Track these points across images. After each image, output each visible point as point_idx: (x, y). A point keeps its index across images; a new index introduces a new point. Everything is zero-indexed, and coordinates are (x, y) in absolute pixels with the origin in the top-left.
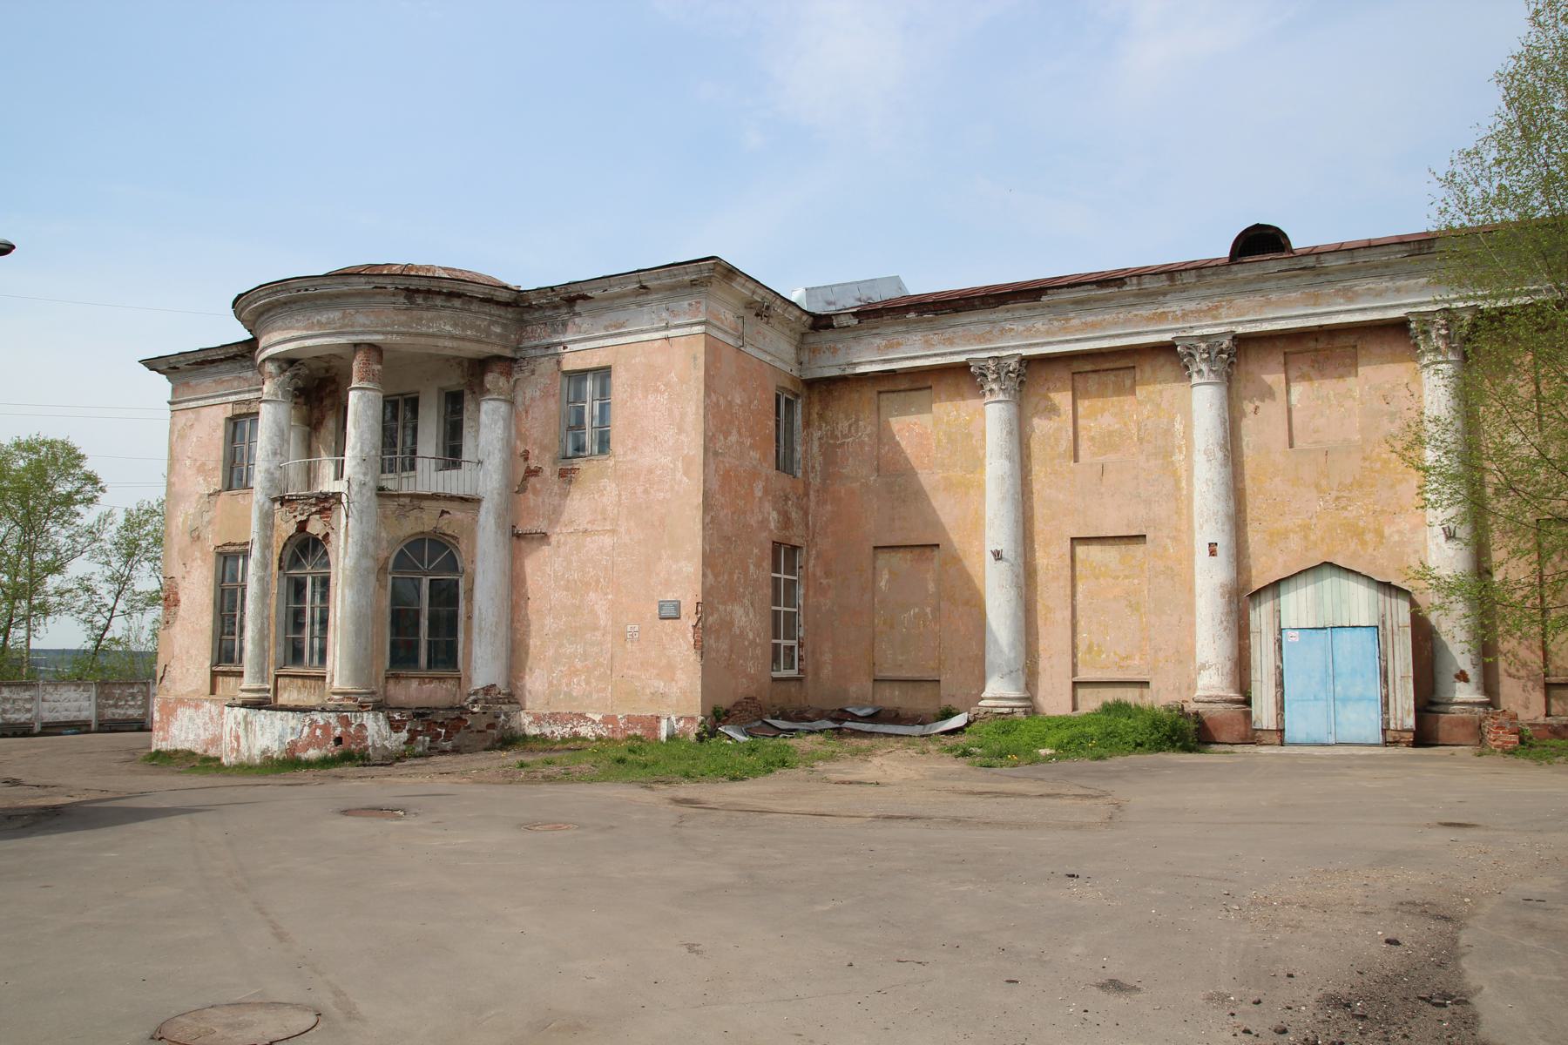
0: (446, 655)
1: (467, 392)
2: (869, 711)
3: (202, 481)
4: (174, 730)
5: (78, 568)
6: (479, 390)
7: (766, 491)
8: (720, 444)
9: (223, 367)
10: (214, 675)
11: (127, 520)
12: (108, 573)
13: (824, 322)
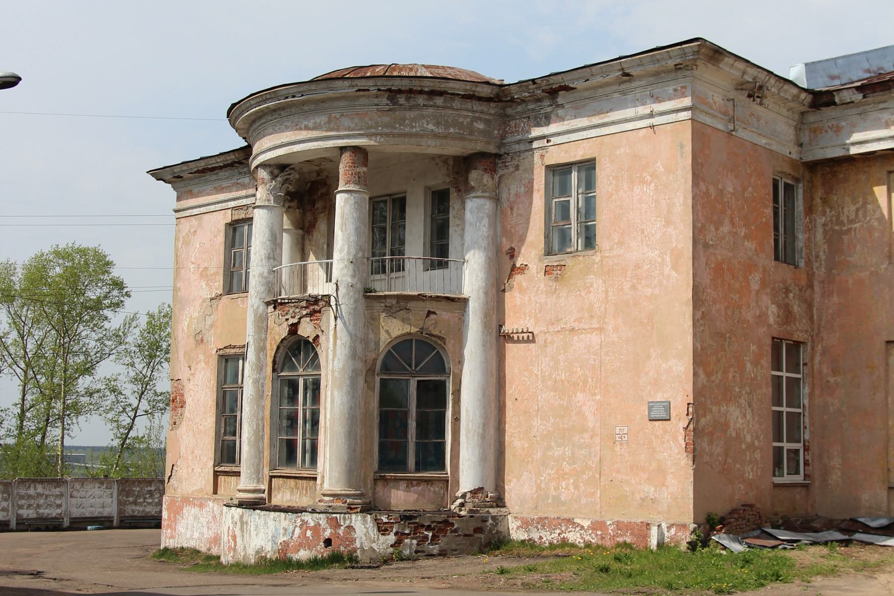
0: (433, 455)
1: (452, 190)
2: (883, 522)
3: (204, 284)
4: (181, 528)
5: (106, 369)
6: (464, 189)
7: (763, 284)
8: (711, 236)
9: (222, 174)
10: (216, 475)
11: (149, 323)
12: (132, 374)
13: (825, 99)
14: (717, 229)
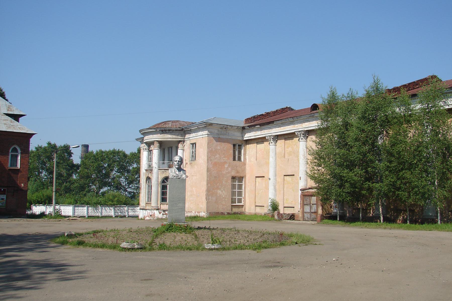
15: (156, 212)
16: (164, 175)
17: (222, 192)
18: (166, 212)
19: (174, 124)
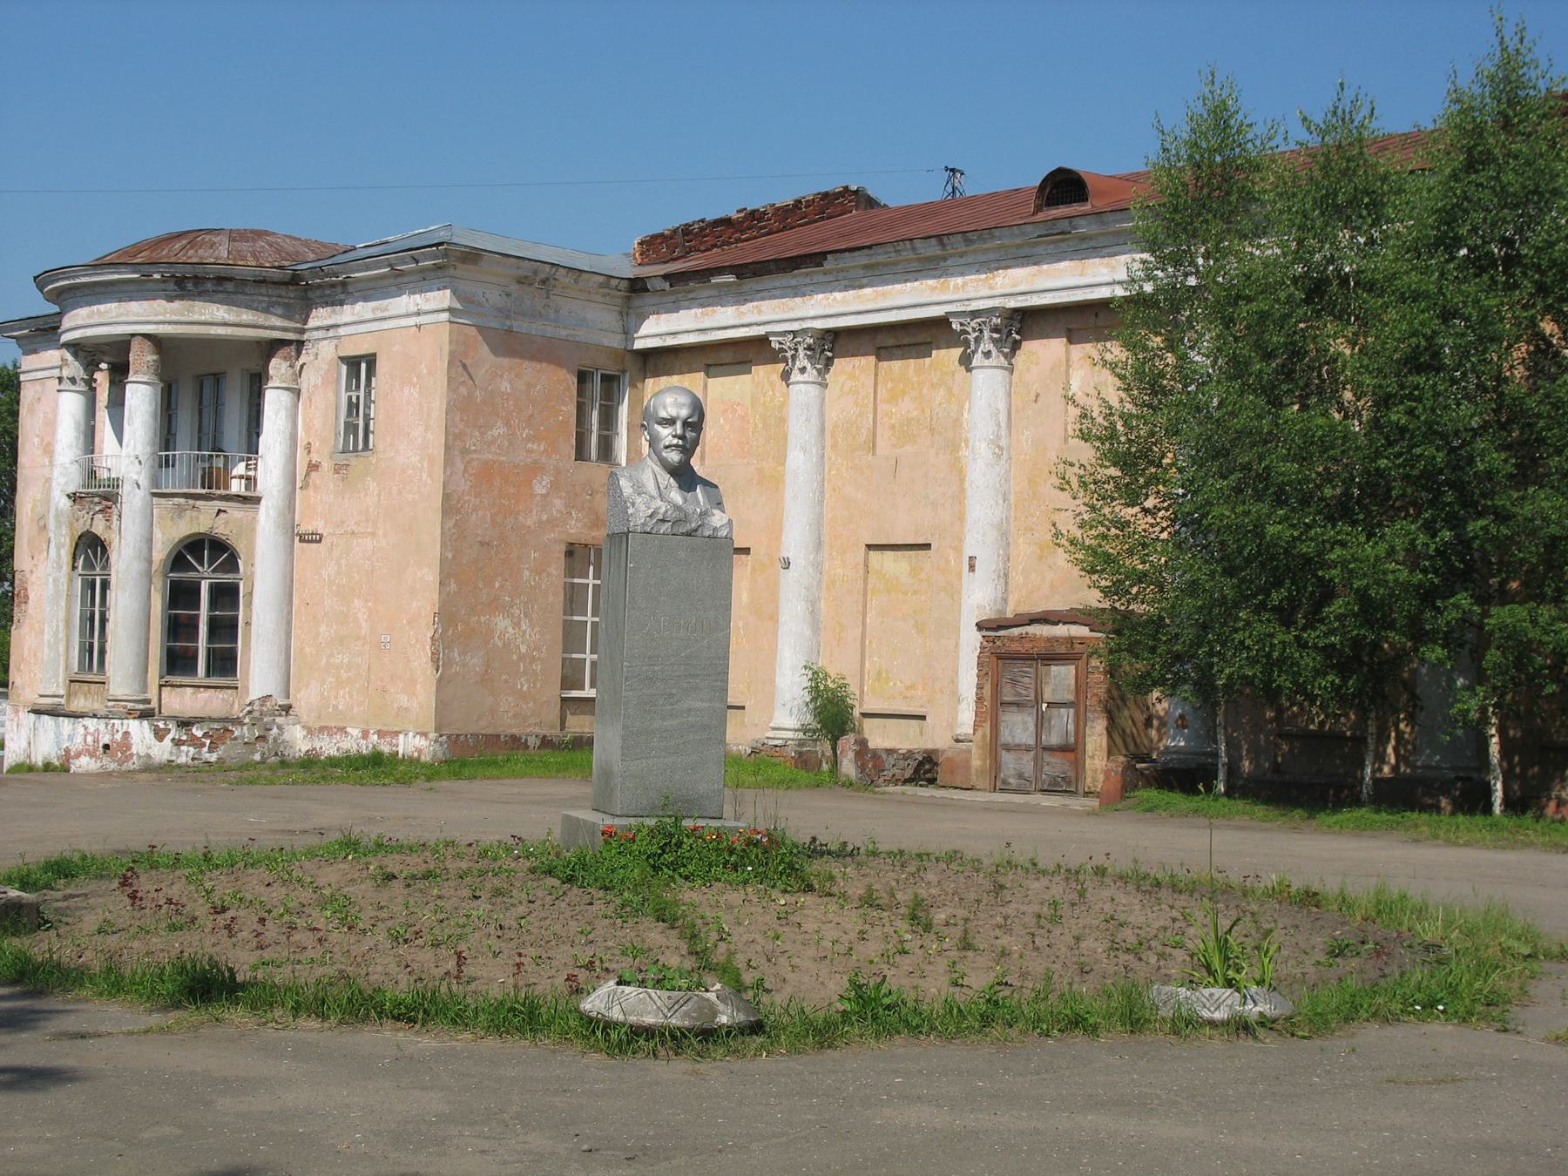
0: (225, 663)
14: (482, 434)
15: (140, 732)
16: (186, 527)
17: (517, 625)
18: (197, 732)
19: (245, 246)
